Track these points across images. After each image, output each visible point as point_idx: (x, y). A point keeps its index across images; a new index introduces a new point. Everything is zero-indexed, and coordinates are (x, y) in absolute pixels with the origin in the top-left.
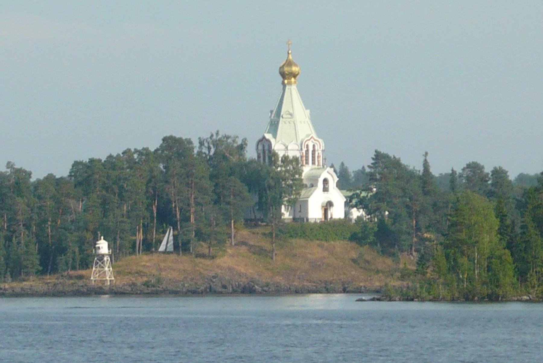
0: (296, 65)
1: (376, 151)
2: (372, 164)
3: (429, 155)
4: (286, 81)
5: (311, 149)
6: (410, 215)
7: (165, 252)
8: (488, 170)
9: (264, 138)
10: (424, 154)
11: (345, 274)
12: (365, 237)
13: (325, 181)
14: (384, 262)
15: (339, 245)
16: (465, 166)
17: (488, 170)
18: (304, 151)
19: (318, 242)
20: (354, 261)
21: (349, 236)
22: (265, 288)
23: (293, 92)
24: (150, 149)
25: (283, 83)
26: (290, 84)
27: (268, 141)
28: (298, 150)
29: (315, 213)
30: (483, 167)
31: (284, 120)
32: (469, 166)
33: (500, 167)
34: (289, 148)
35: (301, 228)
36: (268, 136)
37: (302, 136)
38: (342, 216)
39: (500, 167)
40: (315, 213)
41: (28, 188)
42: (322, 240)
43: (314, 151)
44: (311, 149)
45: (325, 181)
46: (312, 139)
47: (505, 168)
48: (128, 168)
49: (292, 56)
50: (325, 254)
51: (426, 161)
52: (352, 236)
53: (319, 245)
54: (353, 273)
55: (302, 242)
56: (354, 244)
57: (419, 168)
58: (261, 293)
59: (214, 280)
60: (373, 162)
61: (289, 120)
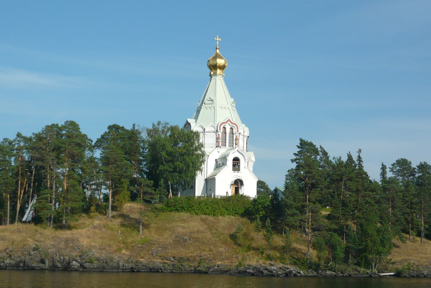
0: (221, 58)
1: (301, 140)
2: (298, 152)
3: (362, 151)
4: (212, 73)
5: (228, 130)
7: (25, 222)
8: (415, 165)
10: (358, 151)
11: (210, 250)
13: (236, 160)
14: (259, 238)
15: (227, 222)
16: (395, 162)
17: (415, 165)
18: (220, 133)
19: (203, 216)
20: (233, 237)
21: (242, 211)
22: (87, 265)
23: (219, 83)
25: (211, 76)
27: (189, 124)
28: (214, 132)
29: (223, 189)
30: (410, 163)
31: (206, 106)
32: (398, 162)
33: (424, 162)
34: (206, 130)
35: (193, 206)
36: (189, 121)
37: (220, 119)
38: (231, 192)
39: (424, 162)
41: (96, 167)
42: (209, 214)
43: (232, 133)
44: (228, 130)
45: (236, 160)
46: (229, 122)
49: (219, 51)
51: (359, 157)
52: (245, 211)
53: (202, 220)
54: (222, 249)
55: (184, 215)
56: (245, 220)
58: (76, 270)
59: (32, 253)
60: (299, 150)
61: (211, 105)
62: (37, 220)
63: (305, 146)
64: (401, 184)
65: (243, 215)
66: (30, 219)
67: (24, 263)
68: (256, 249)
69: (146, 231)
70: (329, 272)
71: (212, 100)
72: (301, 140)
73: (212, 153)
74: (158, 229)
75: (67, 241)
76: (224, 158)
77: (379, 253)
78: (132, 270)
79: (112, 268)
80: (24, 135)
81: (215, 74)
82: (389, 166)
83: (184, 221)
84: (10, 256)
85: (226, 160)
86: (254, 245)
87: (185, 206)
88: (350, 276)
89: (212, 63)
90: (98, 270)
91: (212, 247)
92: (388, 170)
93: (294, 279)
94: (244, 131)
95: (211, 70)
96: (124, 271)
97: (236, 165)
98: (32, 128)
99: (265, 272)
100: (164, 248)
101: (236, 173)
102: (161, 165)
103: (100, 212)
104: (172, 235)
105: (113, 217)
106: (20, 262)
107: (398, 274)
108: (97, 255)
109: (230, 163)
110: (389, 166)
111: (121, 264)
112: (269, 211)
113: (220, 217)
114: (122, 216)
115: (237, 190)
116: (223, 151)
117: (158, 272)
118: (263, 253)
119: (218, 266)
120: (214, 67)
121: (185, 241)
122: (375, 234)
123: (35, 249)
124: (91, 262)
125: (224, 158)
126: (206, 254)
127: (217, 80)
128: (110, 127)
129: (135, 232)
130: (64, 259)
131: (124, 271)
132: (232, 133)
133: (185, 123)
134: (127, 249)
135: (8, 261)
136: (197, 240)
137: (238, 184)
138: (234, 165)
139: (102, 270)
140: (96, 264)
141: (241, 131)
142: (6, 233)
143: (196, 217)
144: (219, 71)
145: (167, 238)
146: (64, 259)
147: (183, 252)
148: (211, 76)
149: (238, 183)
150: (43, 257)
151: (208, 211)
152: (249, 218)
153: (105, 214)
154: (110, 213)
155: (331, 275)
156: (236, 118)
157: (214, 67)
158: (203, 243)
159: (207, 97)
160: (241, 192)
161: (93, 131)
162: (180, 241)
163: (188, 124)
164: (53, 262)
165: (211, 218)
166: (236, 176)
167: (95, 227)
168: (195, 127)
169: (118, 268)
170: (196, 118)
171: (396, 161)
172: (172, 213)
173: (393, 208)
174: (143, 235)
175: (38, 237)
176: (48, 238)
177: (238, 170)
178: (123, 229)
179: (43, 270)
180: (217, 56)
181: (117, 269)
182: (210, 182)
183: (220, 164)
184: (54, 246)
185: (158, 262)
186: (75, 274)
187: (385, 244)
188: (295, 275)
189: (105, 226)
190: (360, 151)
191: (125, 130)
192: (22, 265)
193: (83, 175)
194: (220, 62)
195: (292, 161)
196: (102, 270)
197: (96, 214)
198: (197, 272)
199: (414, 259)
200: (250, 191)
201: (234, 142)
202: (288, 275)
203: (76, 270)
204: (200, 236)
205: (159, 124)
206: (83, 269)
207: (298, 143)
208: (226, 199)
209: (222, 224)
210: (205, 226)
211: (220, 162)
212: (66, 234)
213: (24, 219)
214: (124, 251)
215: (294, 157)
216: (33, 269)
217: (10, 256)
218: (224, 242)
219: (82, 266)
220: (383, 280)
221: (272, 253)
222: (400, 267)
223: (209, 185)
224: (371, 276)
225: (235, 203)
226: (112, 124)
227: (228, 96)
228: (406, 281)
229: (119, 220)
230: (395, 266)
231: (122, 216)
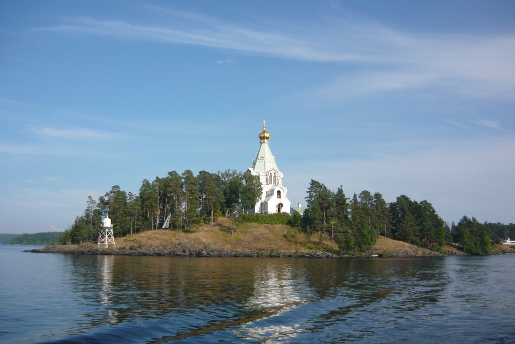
0: (267, 133)
1: (312, 180)
5: (273, 175)
6: (322, 209)
7: (165, 229)
8: (372, 194)
9: (248, 170)
12: (296, 222)
13: (279, 192)
14: (301, 237)
15: (279, 228)
17: (372, 194)
18: (268, 176)
19: (266, 225)
20: (285, 236)
21: (286, 222)
22: (211, 253)
24: (178, 172)
25: (261, 143)
26: (264, 142)
27: (250, 171)
29: (272, 209)
32: (363, 192)
35: (264, 218)
36: (250, 169)
37: (268, 168)
40: (272, 209)
43: (275, 176)
44: (273, 175)
45: (279, 192)
47: (380, 193)
48: (328, 222)
50: (267, 231)
52: (288, 222)
53: (265, 227)
54: (281, 243)
55: (256, 224)
56: (289, 226)
57: (336, 191)
58: (206, 256)
59: (178, 246)
62: (173, 226)
63: (314, 183)
64: (428, 213)
65: (287, 224)
66: (168, 227)
67: (174, 252)
68: (300, 243)
69: (236, 233)
70: (346, 255)
71: (263, 157)
72: (312, 180)
73: (266, 189)
74: (242, 232)
75: (195, 239)
76: (272, 191)
77: (370, 244)
78: (235, 256)
79: (225, 255)
81: (264, 142)
82: (358, 194)
83: (256, 228)
84: (165, 249)
86: (299, 241)
87: (255, 219)
88: (358, 257)
89: (262, 135)
91: (276, 242)
92: (357, 197)
94: (280, 175)
95: (261, 139)
96: (231, 256)
97: (281, 196)
98: (164, 175)
99: (315, 256)
100: (249, 243)
102: (235, 194)
103: (205, 223)
105: (214, 225)
106: (171, 251)
107: (380, 256)
108: (214, 248)
109: (275, 193)
110: (358, 194)
111: (229, 252)
112: (302, 223)
113: (275, 225)
114: (219, 225)
116: (270, 187)
117: (249, 256)
118: (305, 245)
119: (283, 253)
120: (263, 138)
121: (260, 239)
122: (368, 233)
123: (178, 244)
124: (213, 251)
125: (272, 191)
126: (273, 246)
128: (200, 172)
129: (230, 234)
130: (196, 250)
131: (231, 256)
132: (275, 176)
133: (247, 170)
134: (229, 244)
135: (165, 251)
136: (266, 238)
139: (219, 256)
140: (216, 253)
141: (279, 175)
142: (158, 235)
143: (261, 225)
144: (266, 140)
145: (248, 237)
146: (196, 250)
147: (260, 245)
148: (261, 143)
149: (280, 205)
150: (184, 249)
151: (268, 222)
152: (291, 226)
153: (209, 224)
154: (213, 223)
155: (347, 257)
156: (276, 168)
158: (270, 240)
159: (259, 156)
160: (281, 211)
162: (257, 239)
163: (249, 171)
164: (190, 251)
165: (270, 226)
166: (278, 201)
167: (206, 232)
168: (254, 173)
169: (228, 255)
170: (254, 167)
171: (398, 198)
172: (248, 223)
173: (371, 219)
174: (234, 236)
175: (177, 237)
176: (180, 238)
178: (222, 232)
179: (185, 256)
180: (264, 132)
181: (228, 255)
182: (264, 205)
183: (269, 194)
184: (189, 243)
185: (247, 251)
186: (204, 258)
187: (373, 240)
188: (331, 258)
189: (211, 231)
190: (342, 186)
191: (210, 174)
192: (172, 253)
194: (267, 135)
195: (307, 192)
196: (219, 256)
197: (203, 223)
198: (271, 256)
199: (385, 247)
200: (286, 209)
201: (276, 183)
202: (327, 257)
203: (206, 256)
204: (267, 236)
205: (229, 170)
206: (209, 255)
207: (310, 182)
208: (275, 215)
209: (277, 229)
210: (268, 231)
212: (192, 236)
213: (164, 227)
214: (227, 245)
215: (308, 190)
216: (180, 255)
217: (165, 249)
218: (281, 240)
219: (208, 254)
220: (374, 259)
221: (310, 245)
222: (380, 252)
223: (263, 206)
224: (368, 257)
225: (279, 217)
226: (202, 170)
227: (271, 155)
228: (384, 259)
229: (218, 228)
230: (377, 252)
231: (219, 225)
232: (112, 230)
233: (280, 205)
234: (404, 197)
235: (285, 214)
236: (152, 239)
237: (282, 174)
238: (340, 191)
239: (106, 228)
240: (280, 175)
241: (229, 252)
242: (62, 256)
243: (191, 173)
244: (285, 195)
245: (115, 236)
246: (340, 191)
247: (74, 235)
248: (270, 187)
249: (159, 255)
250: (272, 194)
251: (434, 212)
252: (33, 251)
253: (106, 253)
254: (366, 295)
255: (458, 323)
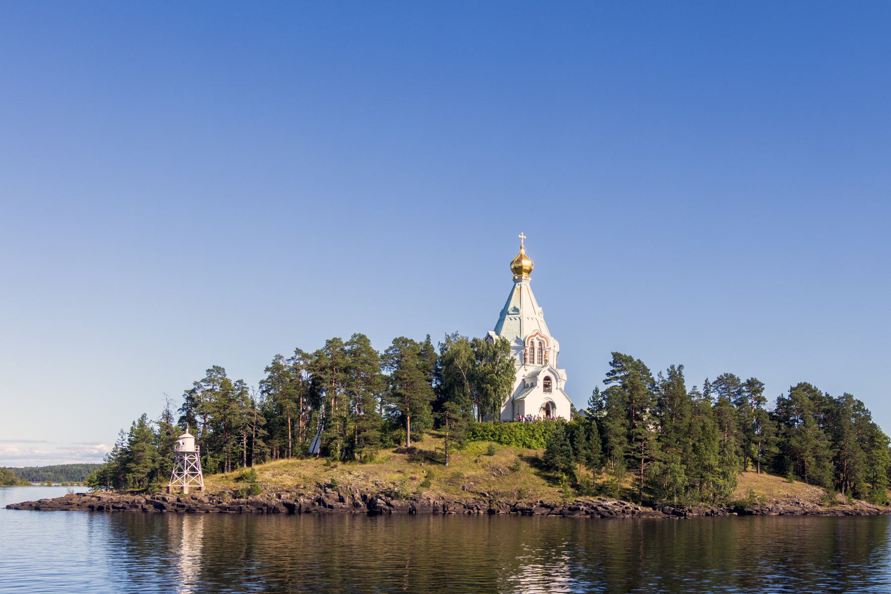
5: (537, 345)
9: (489, 335)
25: (514, 279)
44: (537, 345)
64: (853, 420)
76: (534, 376)
80: (305, 351)
85: (537, 380)
90: (56, 492)
93: (435, 525)
97: (552, 390)
98: (314, 345)
101: (548, 395)
104: (477, 467)
109: (540, 383)
115: (548, 413)
125: (534, 376)
127: (523, 286)
128: (396, 341)
132: (541, 349)
137: (549, 407)
138: (545, 386)
141: (551, 346)
156: (545, 332)
157: (518, 270)
159: (511, 306)
161: (380, 345)
177: (550, 391)
182: (516, 405)
183: (527, 386)
193: (560, 475)
200: (563, 412)
211: (528, 382)
232: (197, 458)
233: (549, 407)
234: (805, 387)
235: (561, 422)
236: (279, 476)
237: (557, 344)
238: (676, 376)
239: (184, 453)
240: (553, 346)
241: (432, 501)
242: (80, 519)
243: (401, 338)
244: (562, 385)
245: (205, 473)
246: (676, 376)
247: (119, 472)
248: (531, 369)
249: (291, 509)
250: (533, 386)
251: (868, 418)
252: (38, 507)
253: (186, 509)
254: (449, 565)
255: (73, 568)
